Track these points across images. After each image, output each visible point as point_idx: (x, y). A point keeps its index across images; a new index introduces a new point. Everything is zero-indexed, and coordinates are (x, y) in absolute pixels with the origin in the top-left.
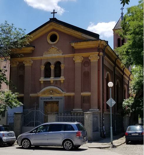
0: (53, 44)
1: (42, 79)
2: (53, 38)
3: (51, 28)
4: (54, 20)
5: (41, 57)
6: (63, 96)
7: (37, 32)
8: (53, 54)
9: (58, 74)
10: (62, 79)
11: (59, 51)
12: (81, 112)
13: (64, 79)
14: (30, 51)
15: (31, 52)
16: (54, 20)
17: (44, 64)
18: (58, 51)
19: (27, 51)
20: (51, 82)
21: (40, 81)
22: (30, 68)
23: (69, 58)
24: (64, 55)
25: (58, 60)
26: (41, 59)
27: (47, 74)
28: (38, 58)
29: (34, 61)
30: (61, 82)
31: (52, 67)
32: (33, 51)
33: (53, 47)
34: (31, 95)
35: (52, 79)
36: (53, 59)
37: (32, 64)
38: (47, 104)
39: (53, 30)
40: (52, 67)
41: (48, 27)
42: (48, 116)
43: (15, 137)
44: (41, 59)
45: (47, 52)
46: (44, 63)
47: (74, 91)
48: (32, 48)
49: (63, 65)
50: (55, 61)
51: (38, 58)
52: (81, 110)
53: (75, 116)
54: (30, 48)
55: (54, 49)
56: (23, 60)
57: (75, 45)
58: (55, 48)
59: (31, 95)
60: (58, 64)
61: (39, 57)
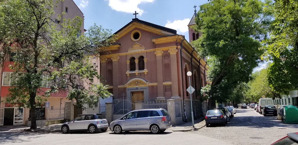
1: (128, 72)
3: (134, 27)
4: (136, 20)
6: (147, 86)
9: (142, 67)
10: (145, 71)
11: (142, 47)
13: (147, 71)
17: (129, 59)
21: (127, 74)
24: (146, 50)
29: (121, 57)
30: (145, 74)
31: (137, 61)
34: (119, 87)
35: (137, 72)
36: (136, 54)
39: (136, 29)
40: (137, 61)
46: (129, 58)
48: (118, 46)
52: (164, 98)
53: (156, 103)
58: (138, 44)
59: (119, 87)
60: (141, 58)
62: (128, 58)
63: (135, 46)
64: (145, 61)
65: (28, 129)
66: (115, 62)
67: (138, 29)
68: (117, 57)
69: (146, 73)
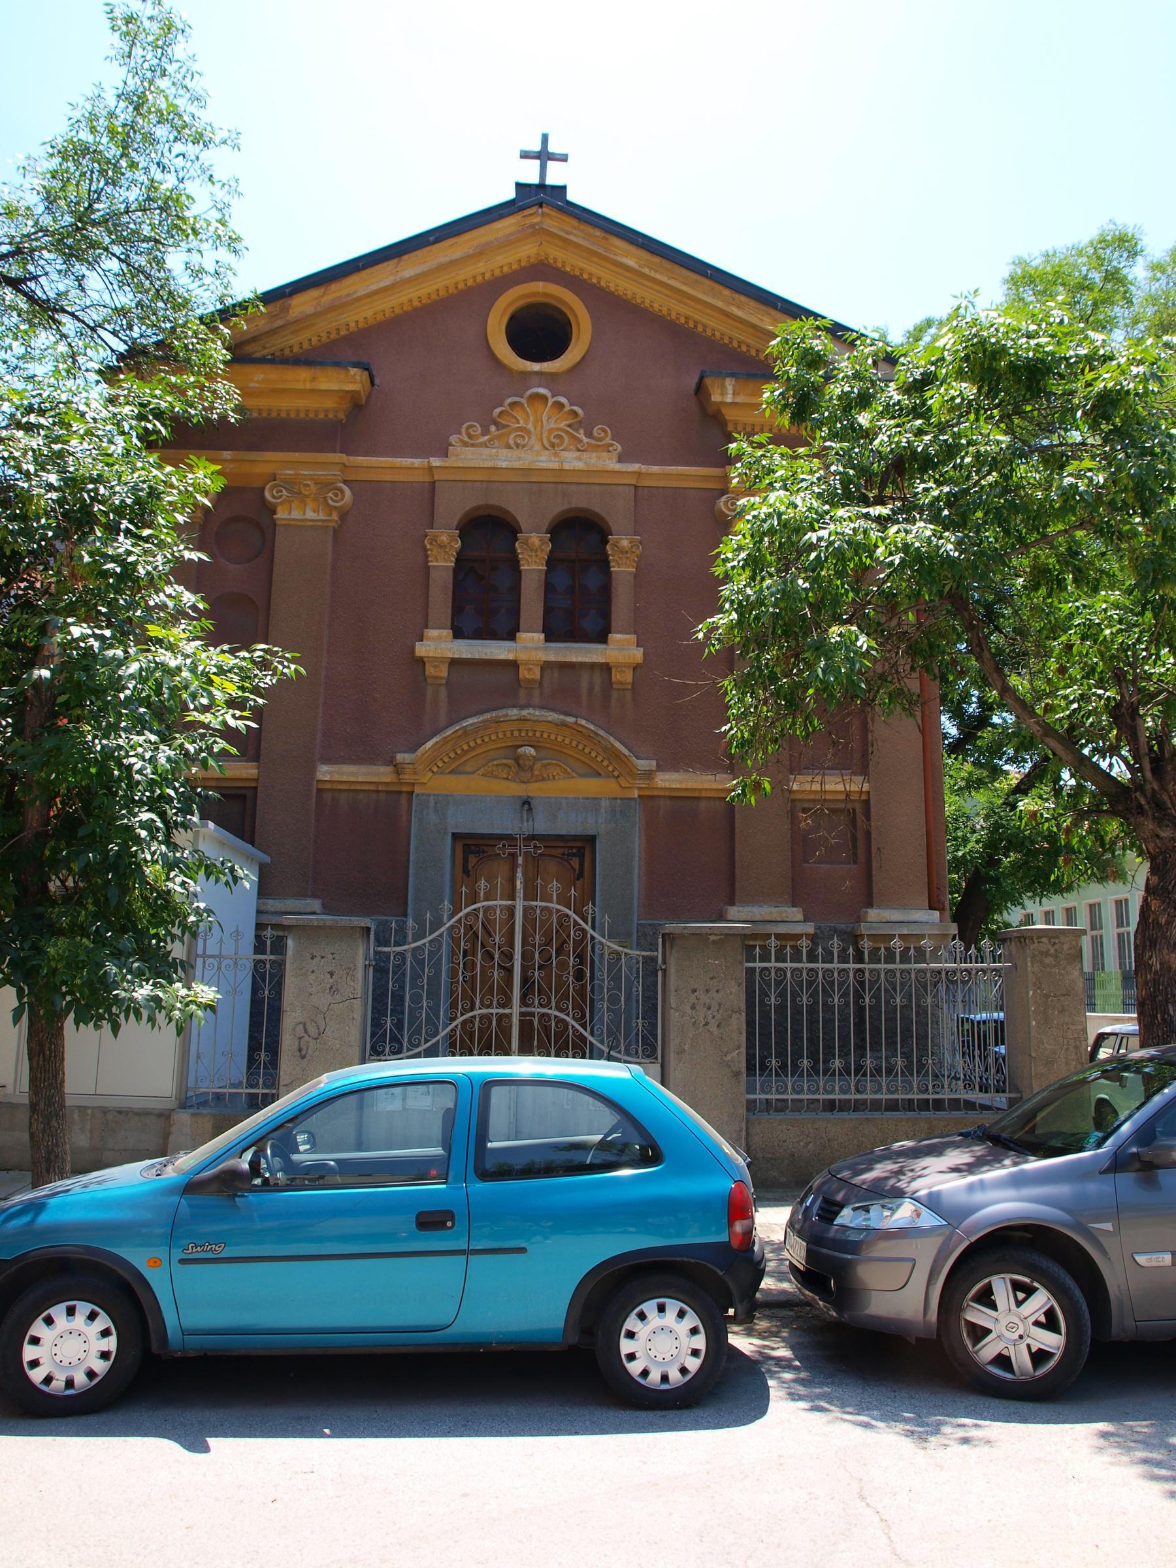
0: (539, 374)
1: (439, 645)
2: (540, 333)
3: (527, 252)
4: (540, 198)
5: (436, 462)
6: (636, 794)
7: (409, 267)
8: (537, 449)
9: (579, 612)
10: (622, 650)
11: (589, 434)
12: (798, 937)
13: (638, 655)
14: (330, 404)
15: (342, 416)
16: (540, 198)
17: (455, 523)
18: (581, 434)
19: (301, 403)
20: (523, 673)
21: (421, 661)
22: (330, 539)
23: (675, 495)
24: (635, 467)
25: (579, 501)
26: (433, 483)
27: (483, 602)
28: (406, 466)
29: (368, 492)
30: (616, 676)
31: (533, 555)
32: (357, 406)
33: (544, 398)
34: (325, 772)
35: (530, 647)
36: (532, 483)
37: (344, 515)
38: (473, 860)
39: (540, 270)
40: (533, 555)
41: (508, 243)
42: (872, 937)
43: (438, 1151)
44: (433, 483)
45: (486, 431)
46: (454, 508)
47: (863, 769)
48: (354, 381)
49: (625, 543)
50: (555, 508)
51: (406, 466)
52: (796, 913)
53: (859, 958)
54: (341, 374)
55: (546, 412)
56: (262, 469)
57: (740, 399)
58: (560, 406)
59: (325, 772)
60: (581, 534)
61: (417, 462)
62: (441, 509)
63: (525, 419)
64: (622, 568)
65: (662, 273)
66: (298, 527)
67: (548, 289)
68: (326, 486)
69: (628, 677)
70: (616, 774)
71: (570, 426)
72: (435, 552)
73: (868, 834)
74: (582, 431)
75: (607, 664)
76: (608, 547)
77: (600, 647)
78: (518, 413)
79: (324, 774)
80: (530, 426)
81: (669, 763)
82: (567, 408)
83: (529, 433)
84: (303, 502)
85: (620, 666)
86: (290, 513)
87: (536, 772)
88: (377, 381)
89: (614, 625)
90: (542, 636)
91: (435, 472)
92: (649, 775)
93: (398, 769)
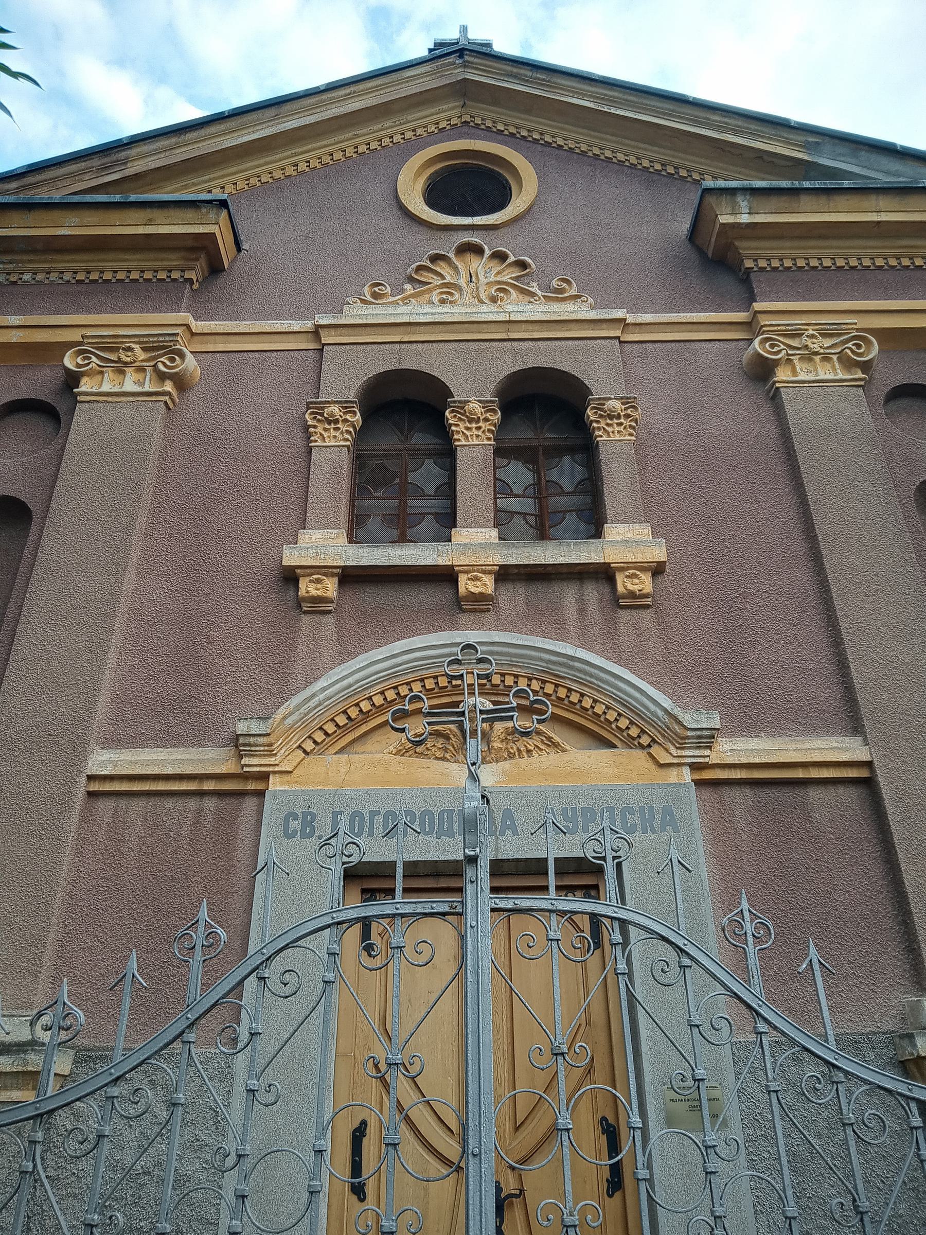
10: (626, 541)
70: (645, 740)
71: (517, 278)
72: (320, 429)
73: (20, 608)
74: (535, 284)
75: (607, 565)
76: (589, 412)
77: (441, 546)
78: (442, 267)
79: (102, 764)
80: (462, 282)
81: (747, 722)
82: (512, 259)
83: (460, 289)
84: (121, 372)
85: (469, 569)
86: (101, 385)
87: (497, 745)
88: (245, 246)
89: (610, 512)
90: (494, 533)
91: (322, 333)
92: (707, 739)
93: (238, 745)
